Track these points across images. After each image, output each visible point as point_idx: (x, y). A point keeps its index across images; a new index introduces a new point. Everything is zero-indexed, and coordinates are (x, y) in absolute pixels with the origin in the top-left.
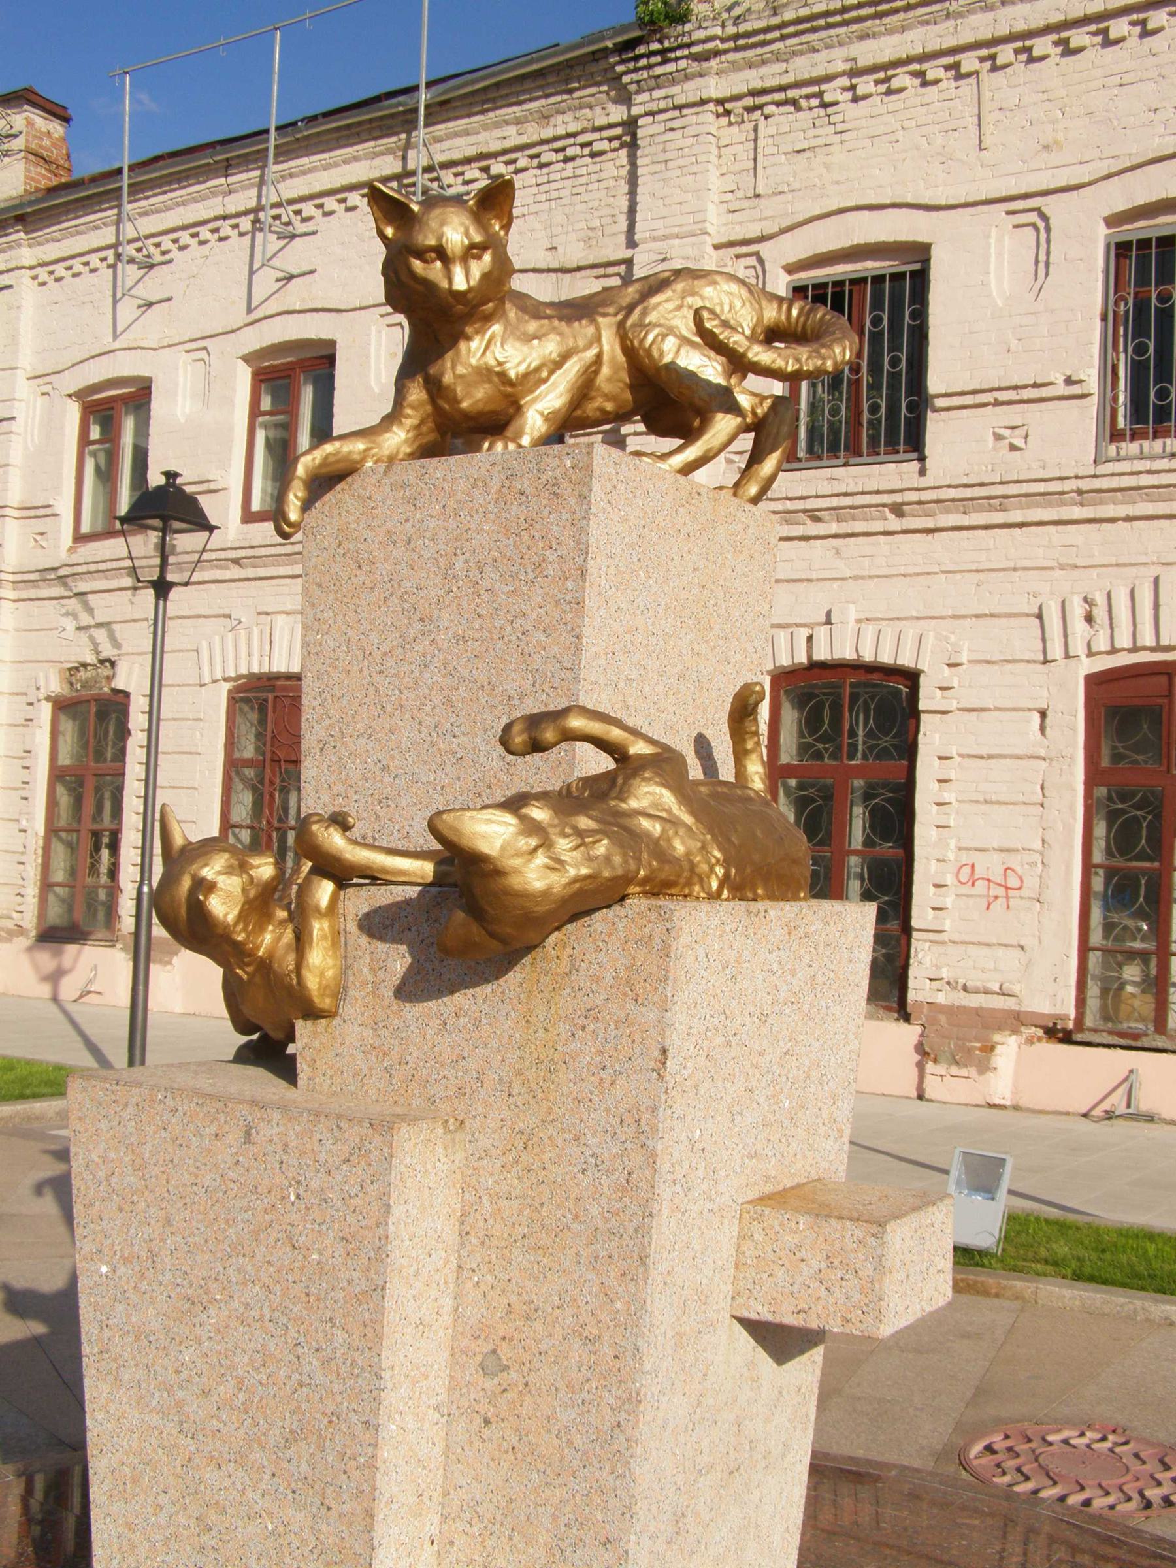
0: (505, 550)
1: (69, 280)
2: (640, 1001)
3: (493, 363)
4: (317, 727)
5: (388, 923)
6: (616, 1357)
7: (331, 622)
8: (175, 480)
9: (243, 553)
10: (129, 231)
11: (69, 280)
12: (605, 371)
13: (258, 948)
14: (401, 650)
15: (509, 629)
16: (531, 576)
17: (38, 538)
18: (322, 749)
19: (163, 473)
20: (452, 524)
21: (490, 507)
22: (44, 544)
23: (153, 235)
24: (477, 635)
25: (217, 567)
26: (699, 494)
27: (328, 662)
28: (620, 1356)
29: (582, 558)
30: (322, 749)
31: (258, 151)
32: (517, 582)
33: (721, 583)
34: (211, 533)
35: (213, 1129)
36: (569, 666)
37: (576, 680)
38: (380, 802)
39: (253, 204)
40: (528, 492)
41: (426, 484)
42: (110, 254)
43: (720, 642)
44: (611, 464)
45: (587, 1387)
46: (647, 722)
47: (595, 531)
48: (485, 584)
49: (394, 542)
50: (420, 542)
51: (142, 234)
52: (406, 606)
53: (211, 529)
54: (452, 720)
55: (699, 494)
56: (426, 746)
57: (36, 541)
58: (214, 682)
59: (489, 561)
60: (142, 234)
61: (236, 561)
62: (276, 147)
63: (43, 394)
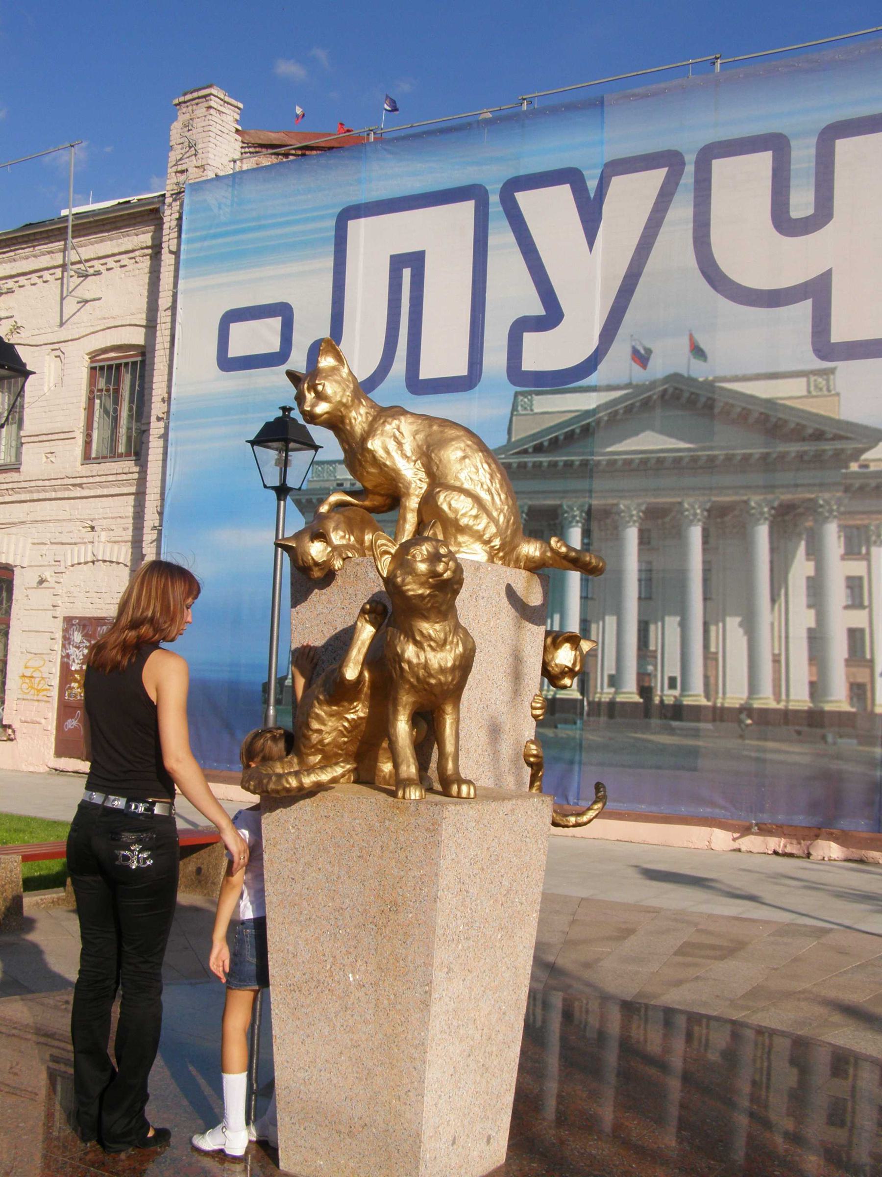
8: (289, 413)
9: (85, 480)
10: (73, 256)
11: (28, 287)
13: (349, 771)
17: (49, 455)
19: (280, 408)
22: (53, 459)
23: (113, 255)
25: (123, 485)
31: (59, 229)
34: (316, 451)
39: (61, 262)
42: (58, 272)
51: (83, 259)
53: (316, 448)
57: (47, 458)
58: (79, 564)
60: (83, 259)
61: (80, 485)
62: (73, 226)
63: (56, 357)
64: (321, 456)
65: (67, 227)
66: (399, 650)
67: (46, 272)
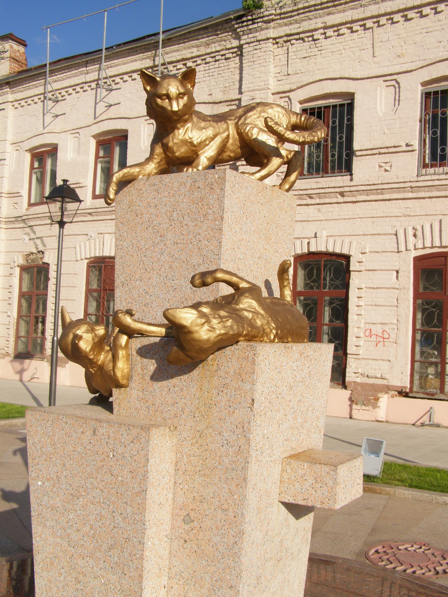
0: (192, 209)
1: (26, 107)
2: (244, 381)
3: (188, 138)
4: (121, 277)
5: (148, 351)
6: (235, 517)
7: (126, 237)
8: (67, 183)
9: (93, 211)
10: (49, 88)
11: (26, 107)
12: (231, 141)
14: (153, 247)
15: (194, 240)
16: (202, 219)
17: (15, 205)
18: (123, 285)
20: (172, 199)
21: (187, 193)
22: (17, 207)
23: (58, 90)
24: (182, 242)
26: (266, 188)
27: (125, 252)
28: (236, 516)
29: (222, 212)
30: (123, 285)
31: (98, 58)
32: (197, 222)
33: (275, 222)
34: (80, 203)
35: (81, 430)
36: (217, 253)
37: (220, 259)
38: (145, 305)
39: (96, 78)
40: (201, 187)
41: (162, 184)
42: (42, 97)
43: (275, 244)
44: (233, 177)
45: (224, 528)
46: (246, 275)
47: (227, 202)
48: (185, 222)
49: (150, 207)
50: (160, 206)
52: (155, 231)
53: (80, 201)
54: (172, 274)
55: (266, 188)
56: (162, 284)
57: (14, 206)
58: (82, 259)
59: (186, 214)
61: (90, 214)
62: (105, 56)
64: (83, 206)
65: (102, 57)
66: (247, 295)
67: (93, 83)
